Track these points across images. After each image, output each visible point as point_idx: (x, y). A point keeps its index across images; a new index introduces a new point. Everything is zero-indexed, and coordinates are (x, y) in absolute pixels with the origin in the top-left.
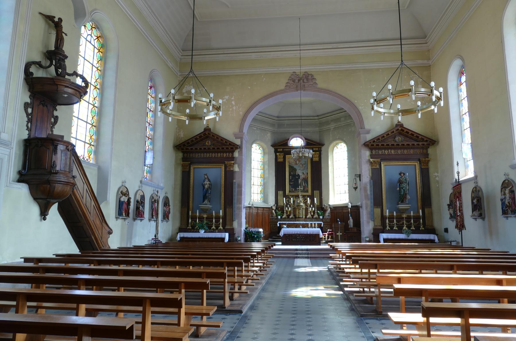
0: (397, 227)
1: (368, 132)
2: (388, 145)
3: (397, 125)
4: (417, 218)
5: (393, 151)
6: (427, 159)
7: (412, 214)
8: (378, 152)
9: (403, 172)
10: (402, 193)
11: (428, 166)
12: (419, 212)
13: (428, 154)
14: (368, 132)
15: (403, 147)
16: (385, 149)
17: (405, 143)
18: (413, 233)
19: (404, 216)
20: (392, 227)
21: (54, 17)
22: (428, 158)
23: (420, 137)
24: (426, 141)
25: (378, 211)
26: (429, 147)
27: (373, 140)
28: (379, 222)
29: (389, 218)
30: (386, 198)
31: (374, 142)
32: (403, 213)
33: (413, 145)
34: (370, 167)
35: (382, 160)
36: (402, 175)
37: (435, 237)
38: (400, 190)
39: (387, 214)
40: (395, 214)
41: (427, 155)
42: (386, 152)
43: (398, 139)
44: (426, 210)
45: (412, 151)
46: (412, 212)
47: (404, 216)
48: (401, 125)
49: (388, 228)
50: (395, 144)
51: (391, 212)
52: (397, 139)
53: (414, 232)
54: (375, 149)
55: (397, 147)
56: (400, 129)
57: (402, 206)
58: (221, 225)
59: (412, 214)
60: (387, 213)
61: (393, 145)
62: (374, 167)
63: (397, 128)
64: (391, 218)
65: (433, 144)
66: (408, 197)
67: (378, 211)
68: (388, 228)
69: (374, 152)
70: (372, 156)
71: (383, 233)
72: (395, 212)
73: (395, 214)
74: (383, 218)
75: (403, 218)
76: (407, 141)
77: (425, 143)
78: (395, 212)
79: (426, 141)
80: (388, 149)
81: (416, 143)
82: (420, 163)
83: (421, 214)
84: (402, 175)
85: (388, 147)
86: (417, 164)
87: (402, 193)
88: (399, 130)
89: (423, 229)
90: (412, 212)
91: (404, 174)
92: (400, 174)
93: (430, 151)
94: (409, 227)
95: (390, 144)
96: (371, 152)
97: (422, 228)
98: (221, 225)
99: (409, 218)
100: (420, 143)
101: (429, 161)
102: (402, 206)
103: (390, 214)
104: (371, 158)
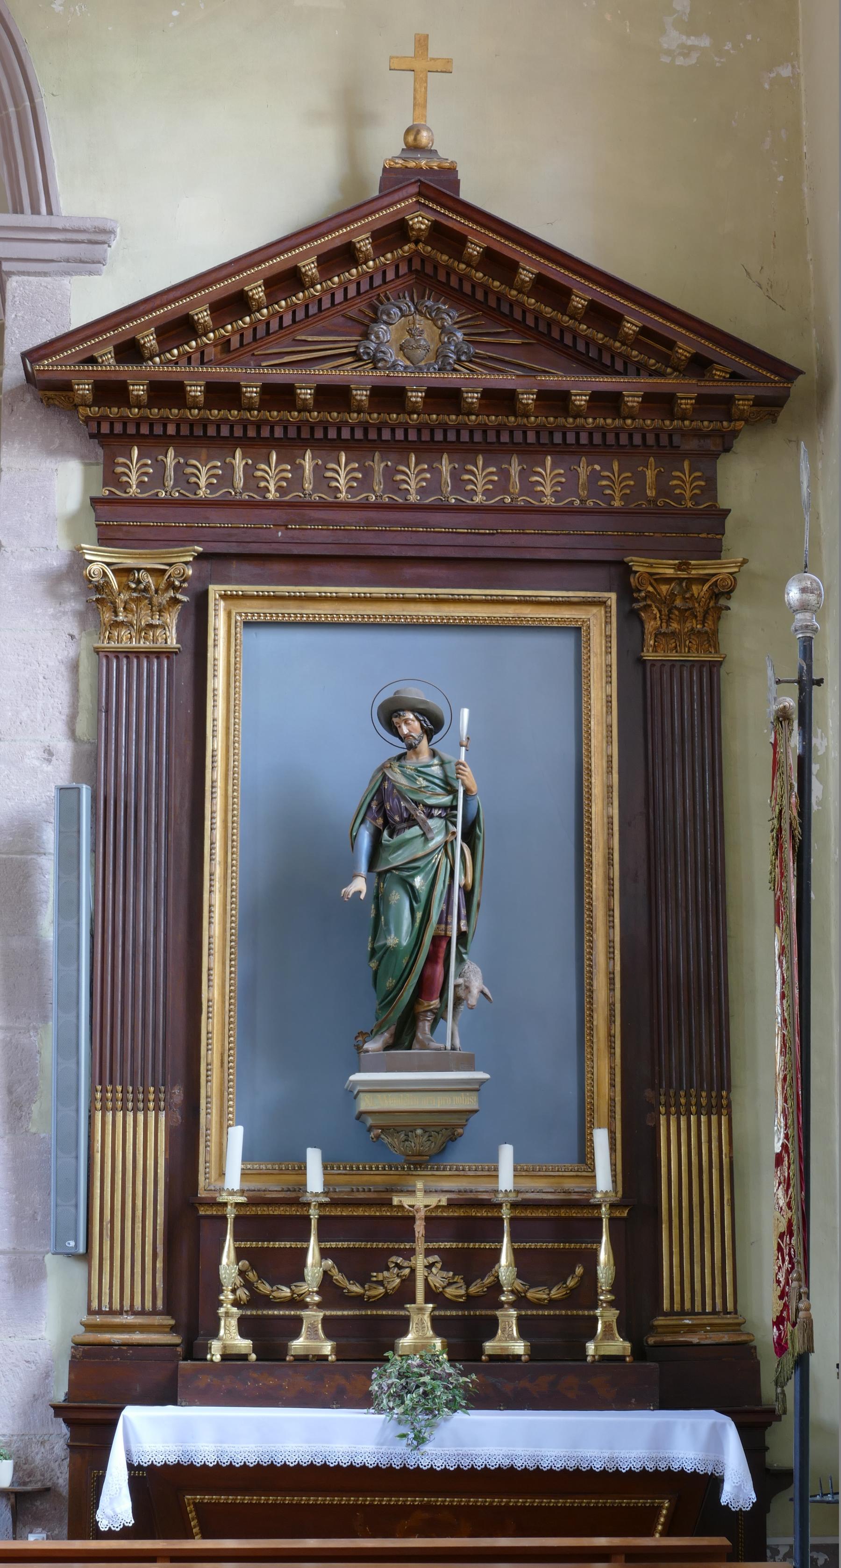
0: (331, 1327)
1: (89, 245)
2: (279, 395)
3: (394, 179)
4: (556, 1228)
5: (343, 475)
6: (699, 568)
7: (506, 1181)
8: (184, 479)
9: (416, 693)
10: (401, 933)
11: (711, 639)
12: (585, 1156)
13: (718, 517)
14: (89, 245)
15: (437, 422)
16: (256, 442)
17: (474, 382)
18: (480, 1400)
19: (420, 1199)
20: (269, 1333)
21: (729, 598)
22: (714, 552)
23: (630, 327)
24: (699, 365)
25: (141, 1138)
26: (726, 443)
27: (123, 335)
28: (140, 1277)
29: (247, 1225)
30: (247, 993)
31: (130, 351)
32: (418, 1163)
33: (555, 401)
34: (87, 643)
35: (214, 561)
36: (411, 725)
37: (716, 1440)
38: (379, 898)
39: (233, 1180)
40: (315, 1181)
41: (704, 527)
42: (272, 475)
43: (413, 343)
44: (675, 1139)
45: (548, 481)
46: (507, 1155)
47: (420, 1199)
48: (437, 186)
49: (230, 1337)
50: (360, 380)
51: (275, 1152)
52: (387, 335)
53: (499, 1388)
54: (153, 440)
55: (386, 421)
56: (420, 222)
57: (389, 1085)
58: (605, 1316)
59: (506, 1181)
60: (230, 1169)
61: (333, 396)
62: (126, 640)
63: (381, 218)
64: (271, 1225)
65: (770, 408)
66: (471, 977)
67: (141, 1138)
68: (230, 1337)
69: (135, 468)
70: (112, 516)
71: (165, 1395)
72: (314, 1158)
73: (315, 1181)
74: (188, 1219)
75: (403, 1224)
76: (494, 364)
77: (686, 390)
78: (314, 1158)
79: (699, 365)
80: (291, 443)
81: (581, 386)
82: (630, 618)
83: (604, 1180)
84: (411, 725)
85: (283, 421)
86: (600, 626)
87: (401, 933)
88: (423, 238)
89: (619, 1346)
90: (507, 1155)
91: (434, 724)
92: (390, 715)
93: (742, 480)
94: (466, 1333)
95: (306, 383)
96: (112, 478)
97: (607, 1343)
98: (605, 1316)
99: (468, 1227)
100: (632, 389)
101: (721, 593)
102: (389, 1085)
103: (272, 1186)
104: (105, 539)
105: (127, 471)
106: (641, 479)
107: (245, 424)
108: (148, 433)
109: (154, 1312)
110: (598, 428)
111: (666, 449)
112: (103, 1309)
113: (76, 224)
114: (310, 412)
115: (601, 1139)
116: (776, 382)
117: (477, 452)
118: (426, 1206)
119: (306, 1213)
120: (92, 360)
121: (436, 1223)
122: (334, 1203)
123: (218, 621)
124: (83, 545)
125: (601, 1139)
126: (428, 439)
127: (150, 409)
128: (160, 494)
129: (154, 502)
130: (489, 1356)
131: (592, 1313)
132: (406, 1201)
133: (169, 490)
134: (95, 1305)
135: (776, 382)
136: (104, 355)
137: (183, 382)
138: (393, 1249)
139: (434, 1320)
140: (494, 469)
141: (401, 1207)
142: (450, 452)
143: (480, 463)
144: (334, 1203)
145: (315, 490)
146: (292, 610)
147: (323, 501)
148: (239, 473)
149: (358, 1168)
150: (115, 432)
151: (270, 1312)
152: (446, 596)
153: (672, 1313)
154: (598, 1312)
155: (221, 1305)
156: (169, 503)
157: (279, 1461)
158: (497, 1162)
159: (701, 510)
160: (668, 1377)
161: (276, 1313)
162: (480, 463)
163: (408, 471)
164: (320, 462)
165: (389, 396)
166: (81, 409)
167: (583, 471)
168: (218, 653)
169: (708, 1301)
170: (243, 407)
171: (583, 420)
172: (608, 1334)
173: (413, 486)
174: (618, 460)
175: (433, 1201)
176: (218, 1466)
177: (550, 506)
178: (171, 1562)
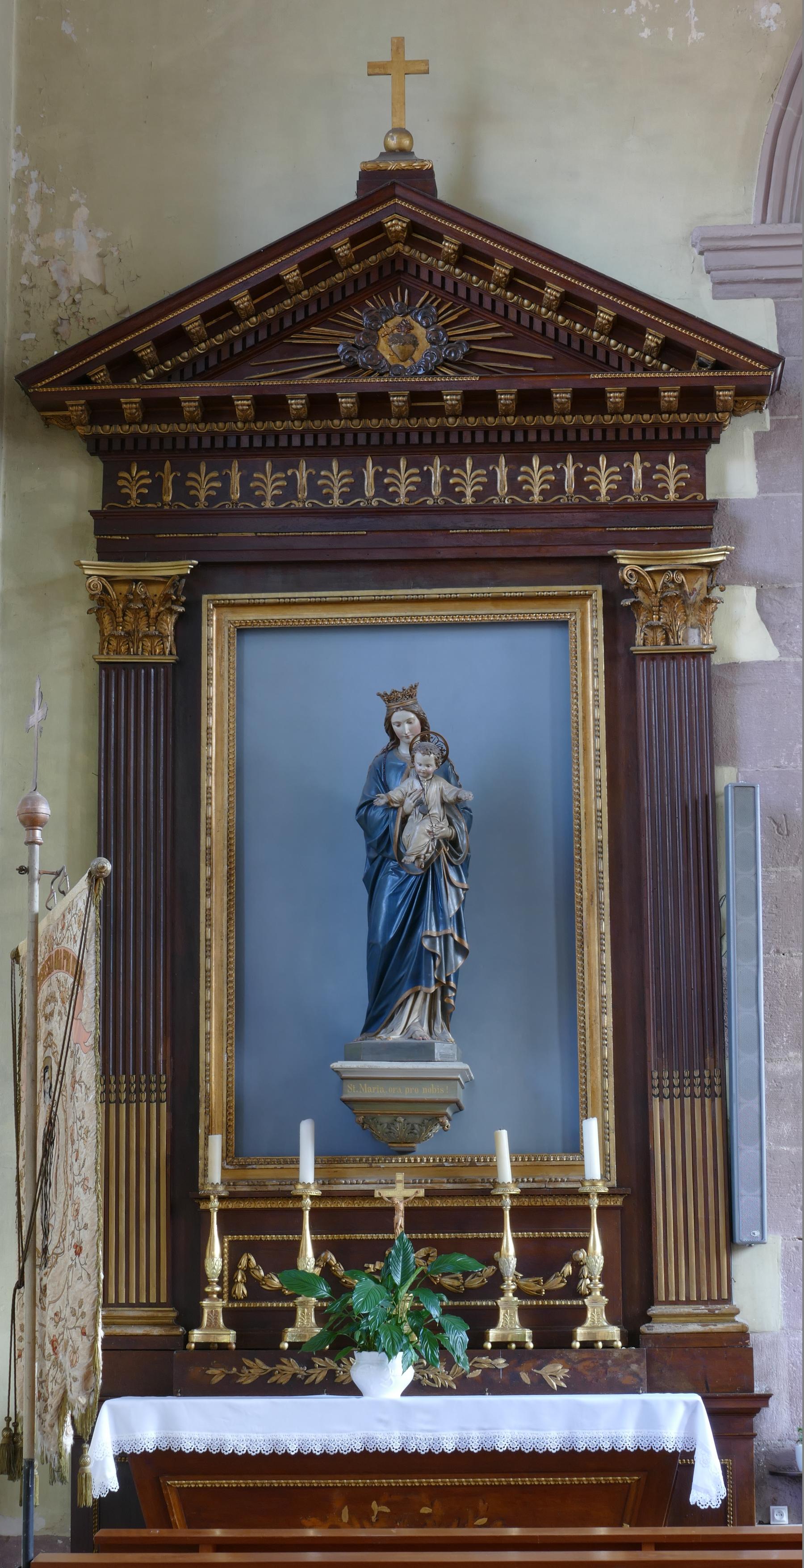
26: (709, 436)
69: (134, 482)
105: (329, 483)
106: (627, 474)
107: (499, 430)
108: (457, 442)
109: (158, 1304)
110: (637, 424)
111: (654, 445)
112: (151, 1301)
113: (720, 233)
114: (197, 423)
115: (591, 1130)
116: (760, 370)
117: (533, 452)
118: (405, 1198)
119: (586, 1204)
120: (86, 380)
121: (416, 1216)
122: (232, 1197)
123: (210, 631)
124: (83, 562)
125: (591, 1130)
126: (561, 439)
127: (679, 414)
128: (698, 498)
129: (423, 510)
130: (196, 1344)
131: (580, 1303)
132: (386, 1193)
133: (303, 500)
134: (112, 1299)
135: (760, 370)
136: (96, 374)
137: (495, 391)
138: (423, 1240)
139: (522, 1310)
140: (416, 471)
141: (381, 1198)
142: (439, 453)
143: (469, 466)
144: (232, 1197)
145: (241, 499)
146: (426, 613)
147: (582, 503)
148: (637, 475)
149: (485, 1161)
150: (372, 443)
151: (473, 1303)
152: (402, 597)
153: (668, 1302)
154: (501, 1301)
155: (502, 1295)
156: (436, 510)
157: (333, 1449)
158: (298, 1155)
159: (481, 506)
160: (660, 1365)
161: (479, 1303)
162: (469, 466)
163: (397, 474)
164: (381, 470)
165: (373, 403)
166: (78, 427)
167: (302, 475)
168: (213, 662)
169: (705, 1289)
170: (663, 409)
171: (195, 426)
172: (212, 1325)
173: (270, 492)
174: (472, 458)
175: (411, 1193)
176: (403, 1452)
177: (338, 508)
178: (656, 1550)
